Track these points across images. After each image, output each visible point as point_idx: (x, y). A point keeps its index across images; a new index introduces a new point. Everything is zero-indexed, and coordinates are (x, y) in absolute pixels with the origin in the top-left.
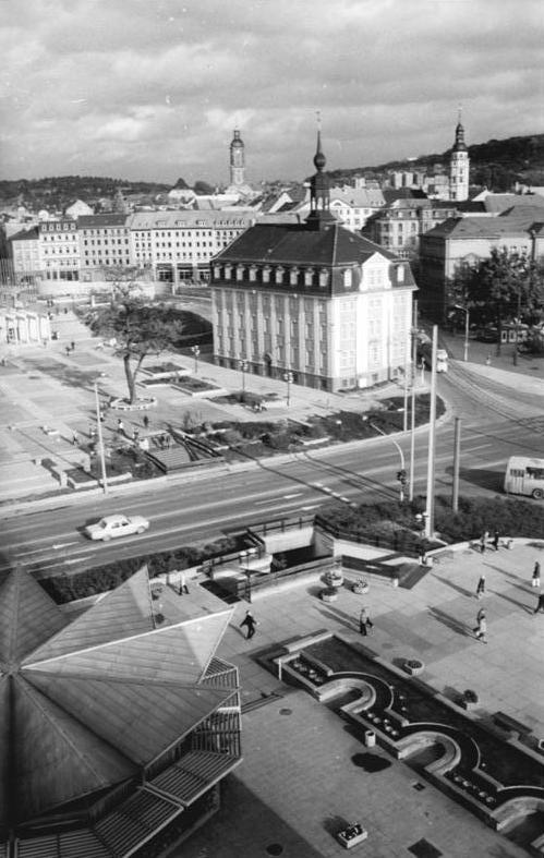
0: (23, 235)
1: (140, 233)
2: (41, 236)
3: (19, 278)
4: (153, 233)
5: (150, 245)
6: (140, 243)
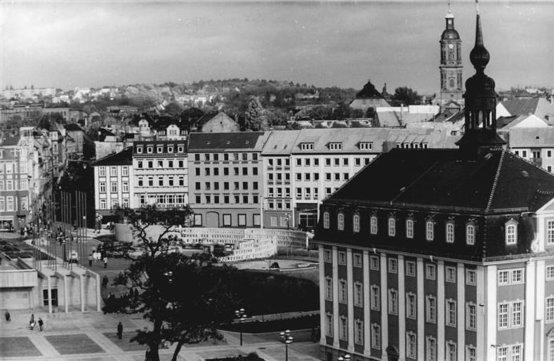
0: (113, 160)
1: (275, 159)
2: (135, 162)
3: (99, 217)
4: (293, 159)
5: (288, 176)
6: (275, 173)
